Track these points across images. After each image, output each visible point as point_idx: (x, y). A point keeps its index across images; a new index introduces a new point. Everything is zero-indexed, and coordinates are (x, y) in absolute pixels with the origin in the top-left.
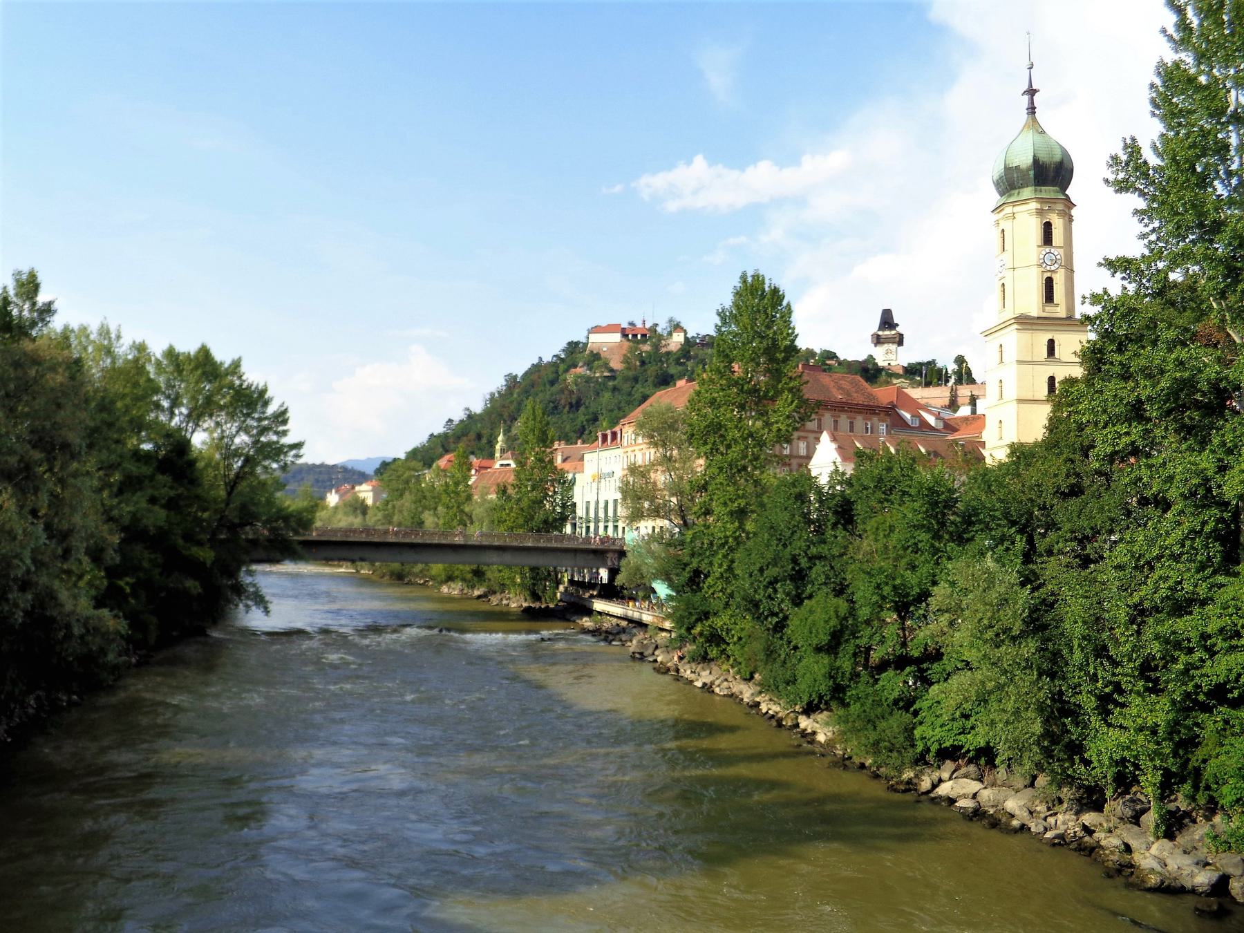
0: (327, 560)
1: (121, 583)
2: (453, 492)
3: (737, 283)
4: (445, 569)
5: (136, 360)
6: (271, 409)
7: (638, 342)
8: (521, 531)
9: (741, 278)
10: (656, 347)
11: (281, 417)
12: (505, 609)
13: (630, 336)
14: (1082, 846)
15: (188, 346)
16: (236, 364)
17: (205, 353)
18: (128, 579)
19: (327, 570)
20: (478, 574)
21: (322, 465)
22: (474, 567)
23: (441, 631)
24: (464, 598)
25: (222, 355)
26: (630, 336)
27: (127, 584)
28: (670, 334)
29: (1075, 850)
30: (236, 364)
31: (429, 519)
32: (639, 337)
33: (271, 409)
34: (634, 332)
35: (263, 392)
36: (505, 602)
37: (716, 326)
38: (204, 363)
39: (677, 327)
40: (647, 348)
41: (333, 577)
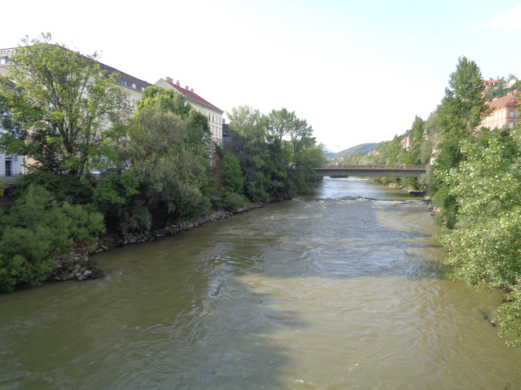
0: (363, 177)
1: (252, 183)
2: (393, 151)
3: (457, 63)
4: (386, 179)
5: (255, 115)
6: (307, 127)
7: (493, 86)
8: (410, 164)
9: (459, 59)
10: (501, 87)
11: (310, 129)
12: (406, 192)
13: (489, 84)
14: (508, 290)
15: (279, 109)
16: (293, 113)
17: (285, 111)
18: (254, 182)
19: (359, 179)
20: (398, 180)
21: (374, 143)
22: (397, 178)
23: (369, 200)
24: (396, 189)
25: (289, 111)
26: (489, 84)
27: (254, 184)
28: (509, 81)
29: (505, 291)
30: (293, 113)
31: (388, 161)
32: (494, 84)
33: (307, 127)
34: (491, 82)
35: (305, 122)
36: (407, 190)
37: (449, 81)
38: (284, 114)
39: (513, 77)
40: (496, 88)
41: (358, 182)
